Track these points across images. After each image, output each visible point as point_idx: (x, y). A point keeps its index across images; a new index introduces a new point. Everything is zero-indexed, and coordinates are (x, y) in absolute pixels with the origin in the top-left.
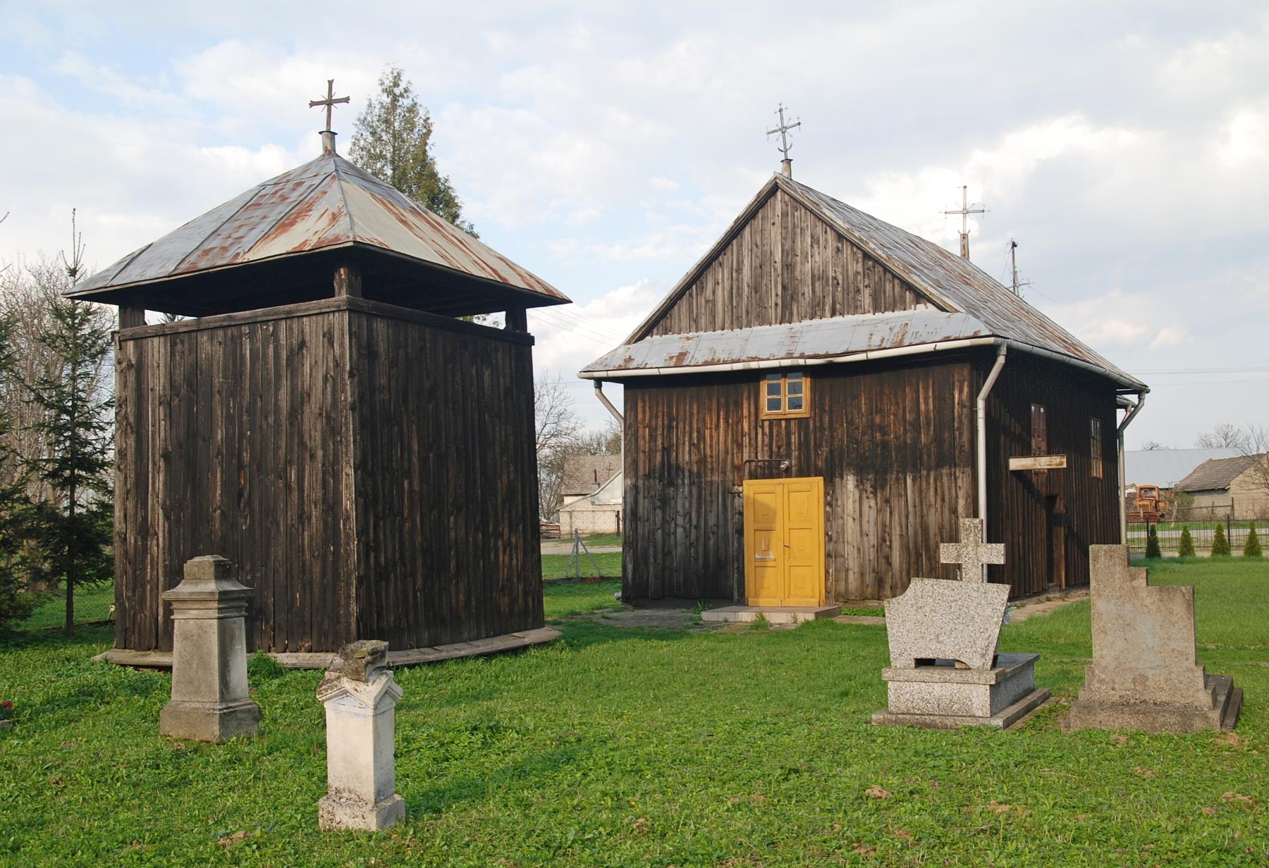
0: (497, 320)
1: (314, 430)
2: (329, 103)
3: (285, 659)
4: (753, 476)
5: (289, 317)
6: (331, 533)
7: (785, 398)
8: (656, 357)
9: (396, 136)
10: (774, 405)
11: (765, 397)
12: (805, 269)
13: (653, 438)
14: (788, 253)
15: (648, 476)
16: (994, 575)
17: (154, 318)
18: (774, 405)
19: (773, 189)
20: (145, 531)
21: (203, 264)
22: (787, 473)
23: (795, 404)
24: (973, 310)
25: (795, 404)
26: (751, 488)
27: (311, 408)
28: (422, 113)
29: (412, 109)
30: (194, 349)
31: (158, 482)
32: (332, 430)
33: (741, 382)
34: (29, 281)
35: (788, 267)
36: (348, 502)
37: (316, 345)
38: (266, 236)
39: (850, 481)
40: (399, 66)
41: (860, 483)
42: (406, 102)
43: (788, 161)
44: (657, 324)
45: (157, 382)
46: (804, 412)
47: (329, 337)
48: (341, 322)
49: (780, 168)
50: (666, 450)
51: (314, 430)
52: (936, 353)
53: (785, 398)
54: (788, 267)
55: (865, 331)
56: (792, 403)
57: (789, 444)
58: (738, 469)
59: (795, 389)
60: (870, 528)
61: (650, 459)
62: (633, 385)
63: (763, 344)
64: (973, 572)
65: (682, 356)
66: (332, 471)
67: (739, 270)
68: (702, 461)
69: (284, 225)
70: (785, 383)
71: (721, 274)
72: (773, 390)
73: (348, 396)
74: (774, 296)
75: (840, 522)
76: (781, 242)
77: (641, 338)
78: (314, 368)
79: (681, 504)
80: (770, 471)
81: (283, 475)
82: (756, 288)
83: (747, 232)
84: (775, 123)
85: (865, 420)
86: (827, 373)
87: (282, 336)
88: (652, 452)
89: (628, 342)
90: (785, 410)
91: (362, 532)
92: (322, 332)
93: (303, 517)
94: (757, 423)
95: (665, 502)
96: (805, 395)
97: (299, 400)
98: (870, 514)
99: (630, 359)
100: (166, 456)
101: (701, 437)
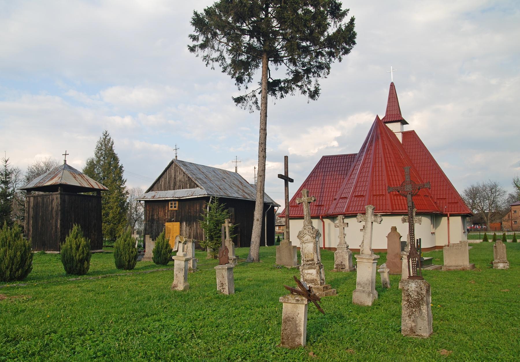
1: (54, 215)
2: (66, 155)
3: (48, 252)
4: (167, 222)
5: (51, 195)
6: (56, 231)
7: (173, 206)
8: (150, 196)
9: (106, 145)
11: (170, 205)
13: (149, 213)
14: (175, 175)
15: (148, 221)
18: (171, 207)
19: (172, 162)
20: (29, 230)
22: (173, 221)
23: (175, 207)
24: (207, 190)
25: (175, 207)
26: (167, 224)
27: (54, 210)
28: (111, 140)
29: (110, 139)
30: (37, 199)
31: (31, 222)
32: (57, 214)
33: (165, 202)
34: (42, 165)
35: (175, 178)
36: (59, 226)
37: (55, 199)
38: (49, 181)
39: (184, 223)
40: (107, 130)
41: (186, 224)
42: (108, 138)
44: (151, 189)
45: (32, 205)
46: (176, 209)
47: (57, 198)
48: (59, 196)
49: (174, 158)
50: (152, 216)
51: (54, 215)
52: (198, 198)
53: (173, 206)
54: (175, 178)
55: (187, 192)
56: (174, 207)
58: (165, 220)
59: (175, 204)
60: (188, 233)
61: (149, 217)
66: (57, 221)
68: (158, 218)
69: (52, 179)
70: (173, 202)
71: (163, 179)
72: (171, 204)
73: (59, 208)
74: (172, 185)
76: (175, 173)
78: (55, 203)
79: (154, 227)
80: (170, 221)
81: (49, 221)
82: (169, 183)
85: (188, 211)
86: (181, 201)
88: (149, 216)
90: (173, 208)
91: (61, 231)
92: (56, 197)
93: (52, 229)
94: (168, 211)
95: (151, 227)
96: (177, 205)
97: (52, 208)
98: (188, 230)
100: (32, 217)
101: (158, 213)
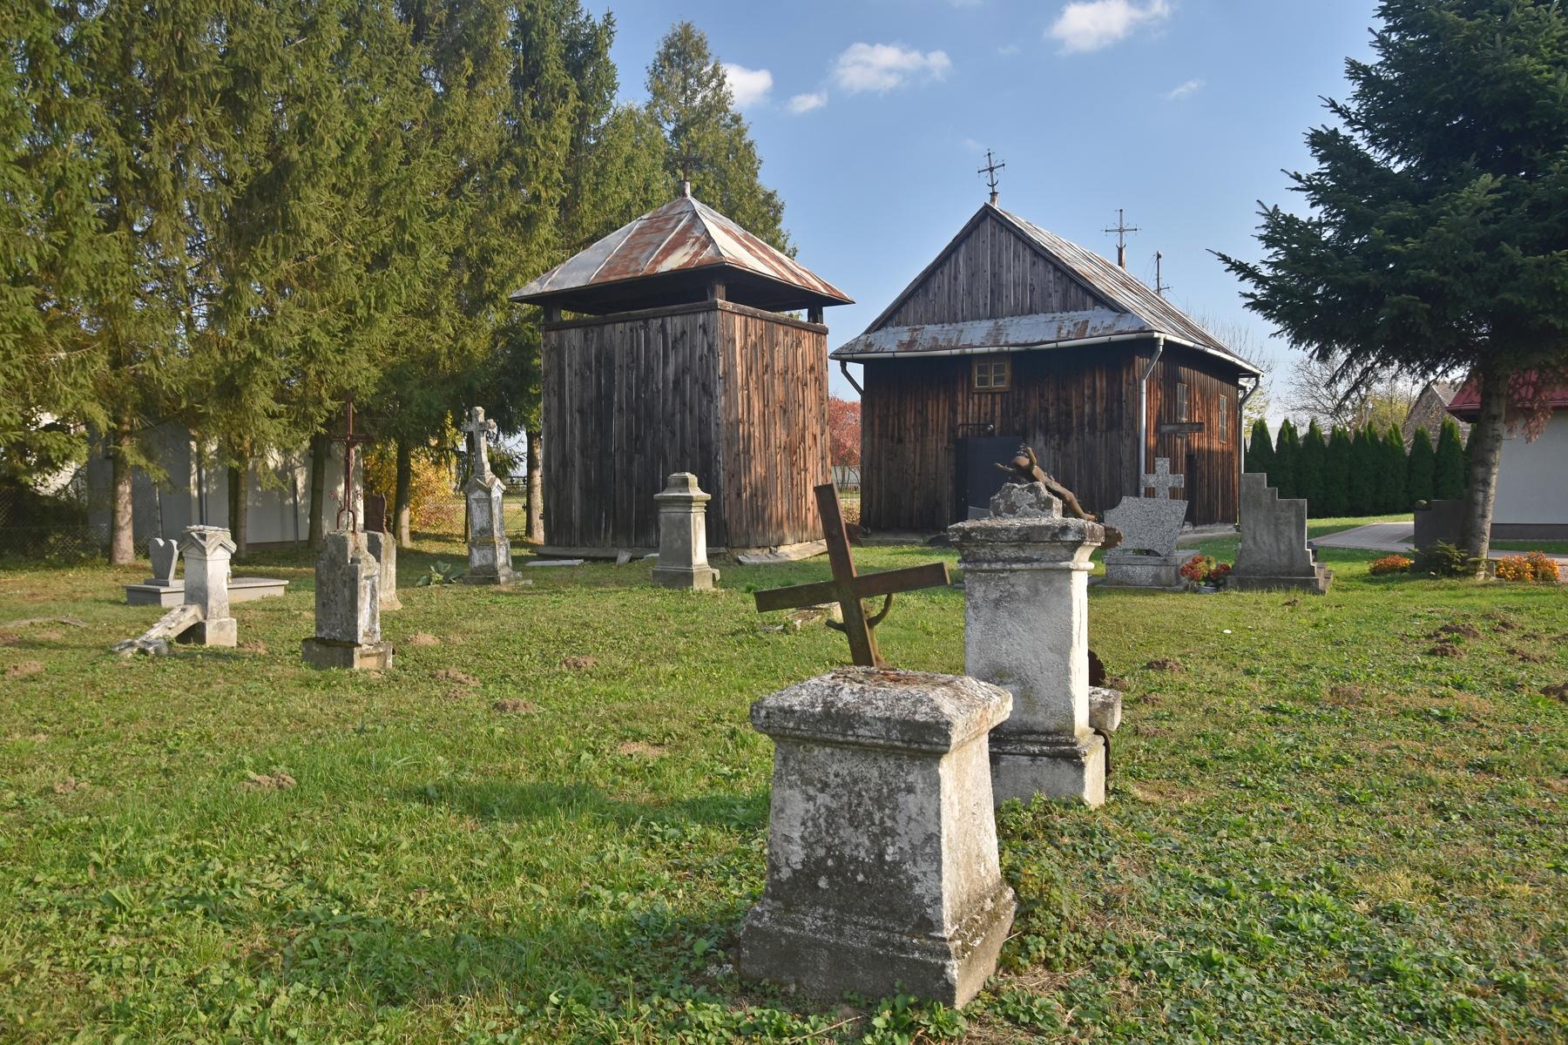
0: (803, 315)
8: (890, 344)
10: (983, 381)
12: (1008, 277)
16: (1174, 494)
17: (567, 316)
21: (612, 278)
43: (993, 194)
52: (1110, 344)
57: (993, 411)
62: (871, 367)
63: (975, 336)
64: (1163, 492)
65: (912, 342)
67: (956, 278)
74: (983, 298)
75: (624, 557)
77: (878, 329)
83: (963, 248)
84: (985, 164)
87: (669, 327)
89: (868, 331)
96: (1007, 373)
99: (871, 345)
